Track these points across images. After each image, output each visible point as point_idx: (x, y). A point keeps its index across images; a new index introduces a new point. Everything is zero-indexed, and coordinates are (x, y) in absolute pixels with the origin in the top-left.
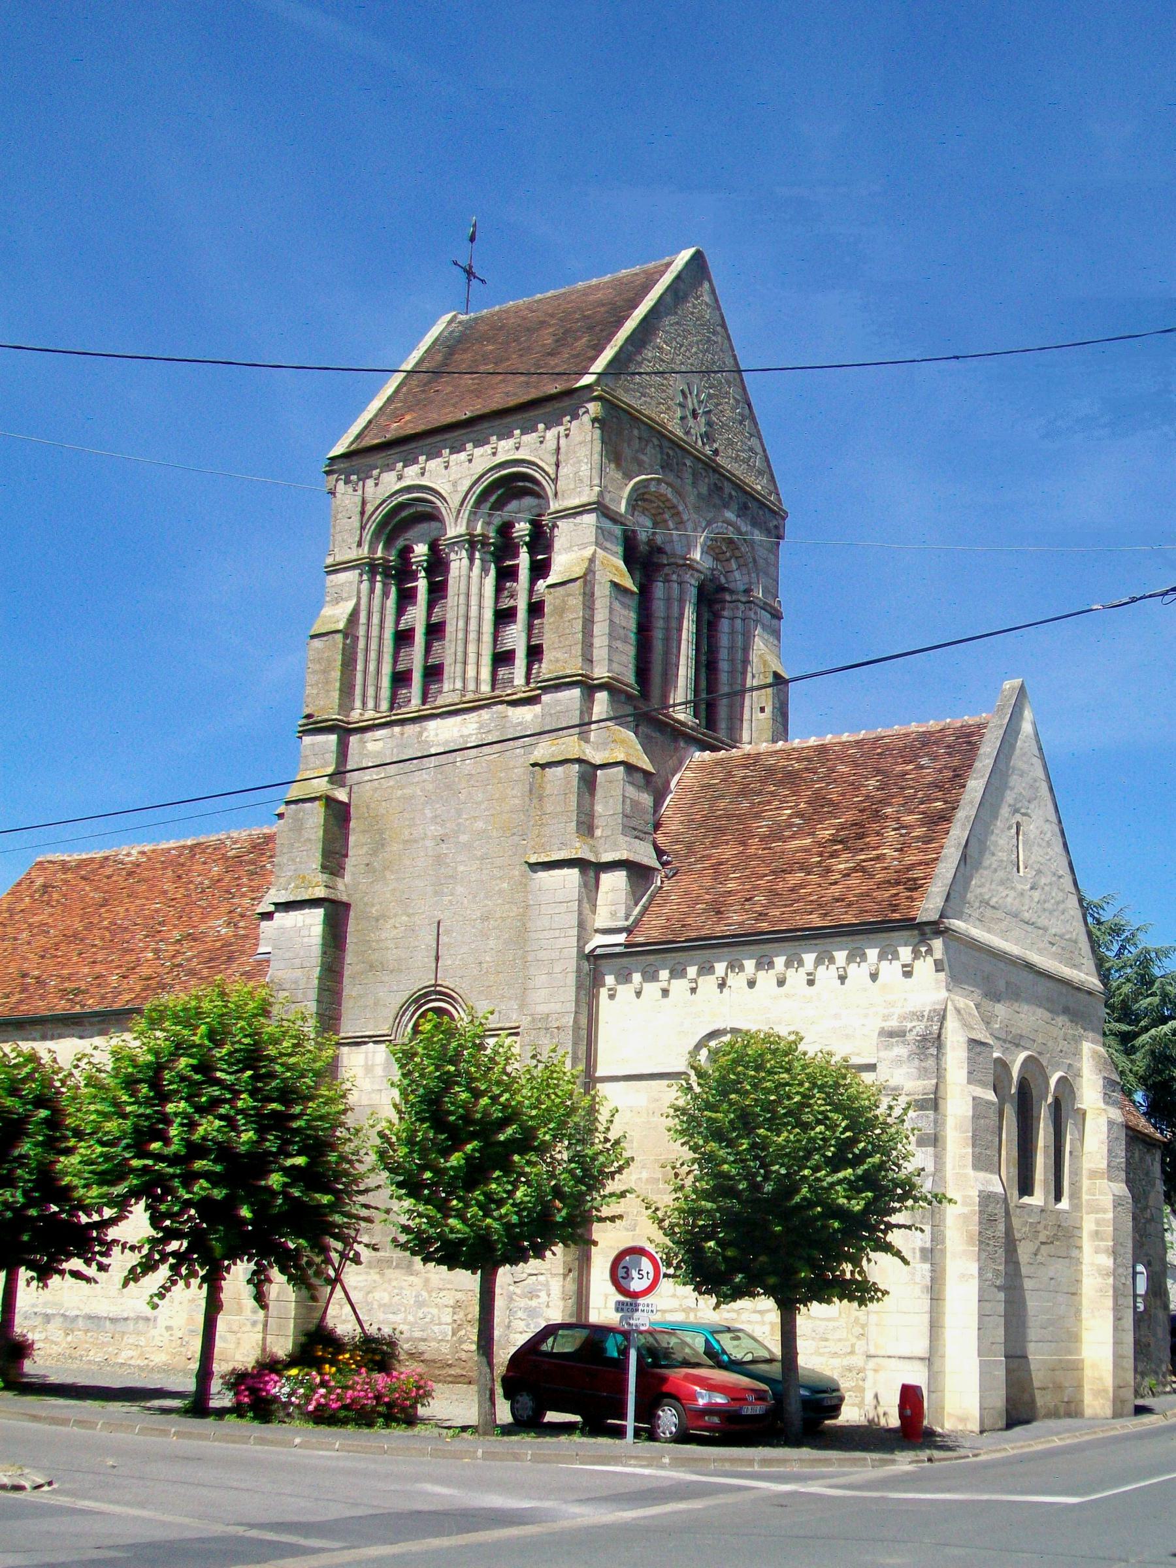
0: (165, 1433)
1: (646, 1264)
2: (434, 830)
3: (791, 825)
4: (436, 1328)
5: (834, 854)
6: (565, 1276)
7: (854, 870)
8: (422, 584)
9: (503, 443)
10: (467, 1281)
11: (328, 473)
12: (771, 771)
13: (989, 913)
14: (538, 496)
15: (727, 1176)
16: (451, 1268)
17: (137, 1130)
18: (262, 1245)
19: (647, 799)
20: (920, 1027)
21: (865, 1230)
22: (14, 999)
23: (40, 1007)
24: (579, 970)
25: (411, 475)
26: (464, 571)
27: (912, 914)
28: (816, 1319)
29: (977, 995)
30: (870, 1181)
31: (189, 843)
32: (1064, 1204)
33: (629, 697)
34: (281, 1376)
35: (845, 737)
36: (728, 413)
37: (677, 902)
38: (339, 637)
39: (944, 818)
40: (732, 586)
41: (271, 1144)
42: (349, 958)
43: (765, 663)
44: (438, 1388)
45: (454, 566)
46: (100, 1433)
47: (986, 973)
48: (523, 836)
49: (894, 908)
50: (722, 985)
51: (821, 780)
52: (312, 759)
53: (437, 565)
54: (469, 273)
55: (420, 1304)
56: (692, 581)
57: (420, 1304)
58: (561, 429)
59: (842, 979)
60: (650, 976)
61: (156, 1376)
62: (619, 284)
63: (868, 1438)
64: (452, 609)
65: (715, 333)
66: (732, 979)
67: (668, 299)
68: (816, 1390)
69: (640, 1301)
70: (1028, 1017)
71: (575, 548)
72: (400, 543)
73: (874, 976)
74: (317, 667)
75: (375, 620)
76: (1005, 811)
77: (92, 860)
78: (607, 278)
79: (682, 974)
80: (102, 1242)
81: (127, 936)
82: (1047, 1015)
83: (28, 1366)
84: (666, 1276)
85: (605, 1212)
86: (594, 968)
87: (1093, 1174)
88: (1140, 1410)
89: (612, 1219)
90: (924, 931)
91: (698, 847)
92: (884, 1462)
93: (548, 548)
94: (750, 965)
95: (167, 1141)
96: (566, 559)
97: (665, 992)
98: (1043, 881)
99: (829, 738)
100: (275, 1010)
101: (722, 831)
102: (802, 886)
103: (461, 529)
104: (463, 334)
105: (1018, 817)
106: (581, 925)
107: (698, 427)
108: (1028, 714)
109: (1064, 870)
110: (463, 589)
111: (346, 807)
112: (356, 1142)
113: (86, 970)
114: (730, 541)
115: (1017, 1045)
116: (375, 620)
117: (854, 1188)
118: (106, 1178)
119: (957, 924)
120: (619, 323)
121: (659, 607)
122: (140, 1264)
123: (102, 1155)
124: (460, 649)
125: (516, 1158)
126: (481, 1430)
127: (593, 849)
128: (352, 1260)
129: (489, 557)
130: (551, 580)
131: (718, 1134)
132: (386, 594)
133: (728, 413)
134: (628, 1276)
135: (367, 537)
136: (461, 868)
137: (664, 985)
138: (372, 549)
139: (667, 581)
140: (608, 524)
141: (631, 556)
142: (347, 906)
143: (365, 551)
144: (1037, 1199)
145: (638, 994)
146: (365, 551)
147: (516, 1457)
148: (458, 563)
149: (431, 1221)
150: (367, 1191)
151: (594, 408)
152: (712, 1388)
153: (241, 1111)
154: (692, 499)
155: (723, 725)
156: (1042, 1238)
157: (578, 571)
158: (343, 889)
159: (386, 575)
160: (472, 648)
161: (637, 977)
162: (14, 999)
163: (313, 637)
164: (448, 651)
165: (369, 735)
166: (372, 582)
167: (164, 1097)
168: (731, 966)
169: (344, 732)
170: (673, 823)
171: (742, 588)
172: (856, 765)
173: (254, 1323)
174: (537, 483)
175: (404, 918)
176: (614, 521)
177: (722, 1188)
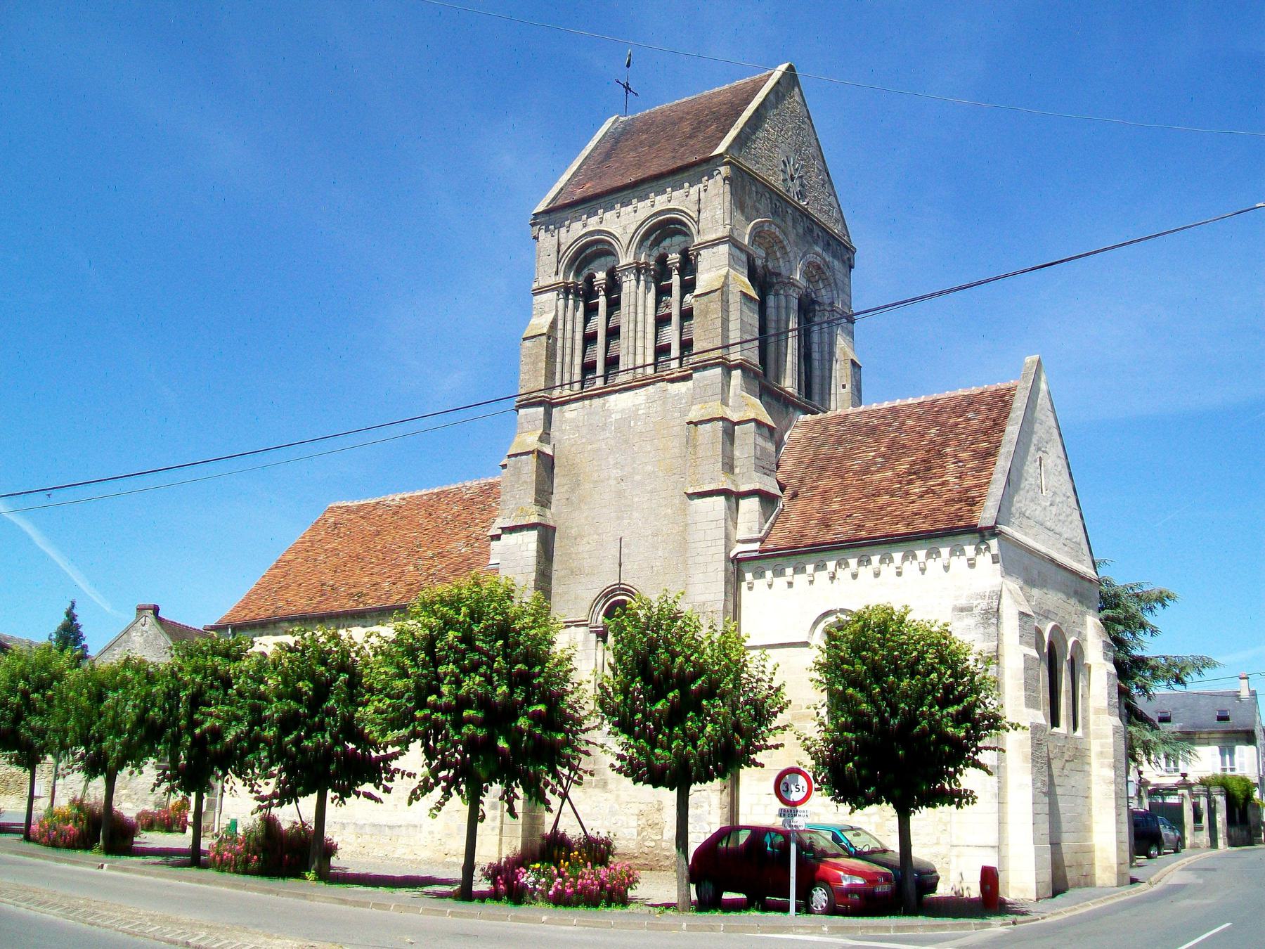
0: (443, 913)
1: (802, 781)
2: (616, 473)
3: (876, 463)
4: (625, 831)
5: (910, 482)
6: (722, 791)
7: (927, 492)
8: (602, 301)
9: (658, 198)
10: (668, 797)
11: (533, 225)
12: (857, 427)
13: (1025, 521)
14: (685, 234)
15: (862, 714)
16: (655, 786)
17: (418, 687)
18: (507, 770)
19: (771, 447)
20: (983, 604)
21: (961, 754)
22: (315, 601)
23: (334, 606)
24: (726, 570)
25: (593, 223)
26: (633, 289)
27: (974, 522)
28: (924, 819)
29: (1020, 582)
30: (964, 716)
31: (436, 490)
32: (1079, 733)
33: (756, 374)
34: (527, 869)
35: (910, 401)
36: (814, 179)
37: (796, 519)
38: (544, 338)
39: (991, 453)
40: (820, 300)
41: (519, 696)
42: (555, 566)
43: (845, 354)
44: (643, 875)
45: (625, 287)
46: (393, 913)
47: (1029, 567)
48: (682, 475)
49: (960, 518)
50: (833, 578)
51: (896, 431)
52: (525, 425)
53: (613, 286)
54: (627, 88)
55: (613, 813)
56: (794, 294)
57: (613, 813)
58: (701, 186)
59: (923, 570)
60: (779, 573)
61: (423, 867)
62: (735, 91)
63: (957, 908)
64: (624, 318)
65: (803, 122)
66: (840, 573)
67: (772, 97)
68: (921, 873)
69: (799, 808)
70: (1053, 599)
71: (714, 269)
72: (586, 272)
73: (946, 568)
74: (528, 360)
75: (569, 326)
76: (1032, 449)
77: (368, 505)
78: (726, 86)
79: (803, 570)
80: (388, 771)
81: (395, 556)
82: (1064, 597)
83: (334, 861)
84: (817, 790)
85: (771, 741)
86: (737, 568)
87: (1098, 711)
88: (1133, 881)
89: (776, 747)
90: (984, 534)
91: (808, 481)
92: (984, 926)
93: (694, 271)
94: (853, 562)
95: (440, 695)
96: (707, 278)
97: (790, 584)
98: (1058, 500)
99: (898, 402)
100: (516, 595)
101: (825, 469)
102: (888, 505)
103: (630, 259)
104: (624, 129)
105: (1040, 454)
106: (727, 537)
107: (795, 187)
108: (1043, 377)
109: (1070, 493)
110: (632, 301)
111: (551, 459)
112: (576, 695)
113: (366, 580)
114: (819, 268)
115: (1047, 618)
116: (569, 326)
117: (958, 720)
118: (394, 724)
119: (1005, 528)
120: (738, 115)
121: (771, 313)
122: (419, 787)
123: (389, 706)
124: (631, 344)
125: (704, 702)
126: (680, 907)
127: (733, 482)
128: (575, 782)
129: (650, 279)
130: (696, 292)
131: (854, 682)
132: (576, 308)
133: (814, 179)
134: (788, 790)
135: (562, 268)
136: (636, 499)
137: (789, 579)
138: (566, 276)
139: (777, 294)
140: (737, 252)
141: (752, 276)
142: (554, 529)
143: (560, 278)
144: (1063, 728)
145: (770, 586)
146: (560, 278)
147: (712, 929)
148: (628, 285)
149: (640, 751)
150: (587, 730)
151: (725, 170)
152: (852, 872)
153: (497, 671)
154: (792, 237)
155: (816, 398)
156: (1066, 757)
157: (717, 285)
158: (550, 517)
159: (577, 295)
160: (640, 343)
161: (769, 574)
162: (315, 601)
163: (525, 339)
164: (623, 347)
165: (566, 407)
166: (566, 299)
167: (436, 662)
168: (839, 564)
169: (549, 405)
170: (788, 466)
171: (827, 301)
172: (920, 419)
173: (493, 829)
174: (685, 225)
175: (596, 537)
176: (741, 250)
177: (860, 721)
